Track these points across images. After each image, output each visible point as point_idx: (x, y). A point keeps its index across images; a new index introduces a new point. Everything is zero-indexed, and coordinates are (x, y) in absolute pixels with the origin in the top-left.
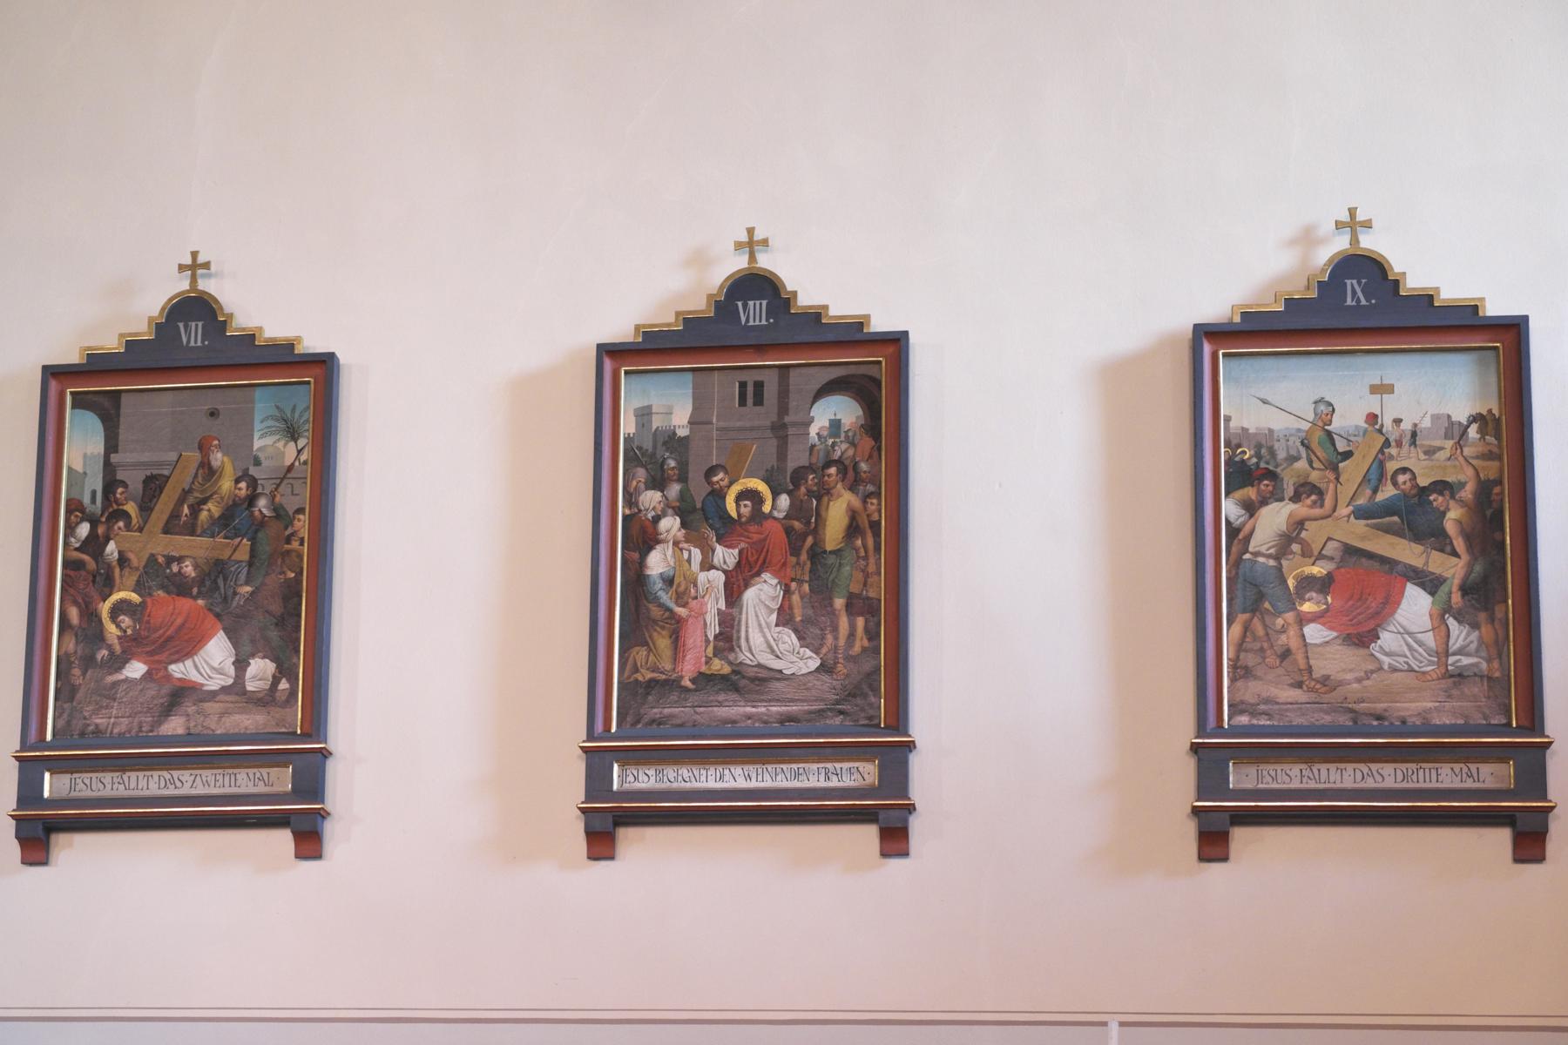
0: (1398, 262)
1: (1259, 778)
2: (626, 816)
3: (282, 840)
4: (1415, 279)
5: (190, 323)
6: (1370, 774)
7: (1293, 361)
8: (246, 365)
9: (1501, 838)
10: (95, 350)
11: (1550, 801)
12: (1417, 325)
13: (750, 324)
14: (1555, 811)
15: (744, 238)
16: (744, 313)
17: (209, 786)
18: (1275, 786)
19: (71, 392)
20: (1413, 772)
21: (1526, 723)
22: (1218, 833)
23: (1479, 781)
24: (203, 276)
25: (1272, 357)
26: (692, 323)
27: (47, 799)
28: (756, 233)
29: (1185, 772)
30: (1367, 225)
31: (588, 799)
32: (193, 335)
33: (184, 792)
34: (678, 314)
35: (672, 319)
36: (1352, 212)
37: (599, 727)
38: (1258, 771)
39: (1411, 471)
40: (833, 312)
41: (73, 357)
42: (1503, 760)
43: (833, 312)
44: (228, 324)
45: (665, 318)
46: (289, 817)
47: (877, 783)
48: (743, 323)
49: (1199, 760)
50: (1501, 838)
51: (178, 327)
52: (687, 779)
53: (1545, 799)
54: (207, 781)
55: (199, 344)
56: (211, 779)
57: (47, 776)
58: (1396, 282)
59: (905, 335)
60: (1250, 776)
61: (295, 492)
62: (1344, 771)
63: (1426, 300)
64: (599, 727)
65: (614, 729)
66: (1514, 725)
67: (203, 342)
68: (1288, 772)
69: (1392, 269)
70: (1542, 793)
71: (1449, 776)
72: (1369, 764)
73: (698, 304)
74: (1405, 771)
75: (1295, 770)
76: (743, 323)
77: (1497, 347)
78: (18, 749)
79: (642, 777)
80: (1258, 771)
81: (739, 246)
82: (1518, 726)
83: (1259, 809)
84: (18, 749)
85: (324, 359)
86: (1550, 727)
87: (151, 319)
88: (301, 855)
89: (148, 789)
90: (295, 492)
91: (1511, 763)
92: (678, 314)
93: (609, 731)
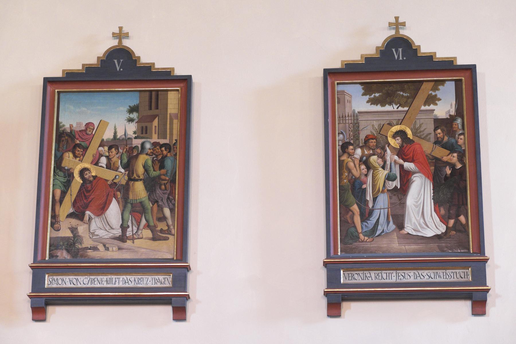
0: (417, 41)
1: (398, 276)
2: (53, 300)
3: (465, 306)
4: (425, 49)
5: (399, 49)
6: (71, 281)
7: (81, 96)
8: (443, 70)
9: (168, 310)
10: (358, 62)
11: (488, 286)
12: (430, 69)
13: (400, 59)
14: (490, 292)
15: (393, 20)
16: (397, 55)
17: (441, 278)
18: (405, 281)
19: (58, 91)
20: (93, 280)
21: (179, 258)
22: (336, 303)
23: (379, 279)
24: (401, 28)
25: (77, 93)
26: (369, 60)
27: (342, 284)
28: (123, 29)
29: (322, 274)
30: (127, 36)
31: (32, 292)
32: (398, 54)
33: (393, 281)
34: (83, 65)
35: (359, 58)
36: (397, 18)
37: (39, 258)
38: (396, 273)
39: (114, 145)
40: (438, 56)
41: (337, 65)
42: (167, 273)
43: (438, 56)
44: (418, 51)
45: (77, 66)
46: (171, 299)
47: (470, 279)
48: (118, 70)
49: (327, 269)
50: (168, 310)
51: (392, 51)
52: (463, 276)
53: (485, 285)
54: (55, 282)
55: (401, 59)
56: (384, 276)
57: (47, 276)
58: (136, 60)
59: (474, 66)
60: (149, 281)
61: (380, 133)
62: (392, 274)
63: (430, 58)
64: (39, 258)
65: (339, 254)
66: (471, 252)
67: (403, 58)
68: (409, 274)
69: (414, 44)
70: (185, 289)
71: (67, 281)
72: (418, 271)
73: (93, 60)
74: (378, 274)
75: (431, 273)
76: (118, 70)
77: (179, 89)
78: (32, 263)
79: (356, 276)
80: (396, 273)
81: (114, 35)
82: (473, 253)
83: (376, 292)
84: (32, 263)
85: (471, 68)
86: (487, 253)
87: (377, 48)
88: (176, 319)
89: (392, 279)
90: (380, 133)
91: (470, 269)
92: (362, 56)
93: (45, 259)
